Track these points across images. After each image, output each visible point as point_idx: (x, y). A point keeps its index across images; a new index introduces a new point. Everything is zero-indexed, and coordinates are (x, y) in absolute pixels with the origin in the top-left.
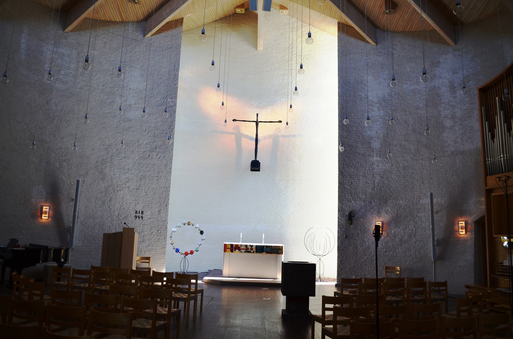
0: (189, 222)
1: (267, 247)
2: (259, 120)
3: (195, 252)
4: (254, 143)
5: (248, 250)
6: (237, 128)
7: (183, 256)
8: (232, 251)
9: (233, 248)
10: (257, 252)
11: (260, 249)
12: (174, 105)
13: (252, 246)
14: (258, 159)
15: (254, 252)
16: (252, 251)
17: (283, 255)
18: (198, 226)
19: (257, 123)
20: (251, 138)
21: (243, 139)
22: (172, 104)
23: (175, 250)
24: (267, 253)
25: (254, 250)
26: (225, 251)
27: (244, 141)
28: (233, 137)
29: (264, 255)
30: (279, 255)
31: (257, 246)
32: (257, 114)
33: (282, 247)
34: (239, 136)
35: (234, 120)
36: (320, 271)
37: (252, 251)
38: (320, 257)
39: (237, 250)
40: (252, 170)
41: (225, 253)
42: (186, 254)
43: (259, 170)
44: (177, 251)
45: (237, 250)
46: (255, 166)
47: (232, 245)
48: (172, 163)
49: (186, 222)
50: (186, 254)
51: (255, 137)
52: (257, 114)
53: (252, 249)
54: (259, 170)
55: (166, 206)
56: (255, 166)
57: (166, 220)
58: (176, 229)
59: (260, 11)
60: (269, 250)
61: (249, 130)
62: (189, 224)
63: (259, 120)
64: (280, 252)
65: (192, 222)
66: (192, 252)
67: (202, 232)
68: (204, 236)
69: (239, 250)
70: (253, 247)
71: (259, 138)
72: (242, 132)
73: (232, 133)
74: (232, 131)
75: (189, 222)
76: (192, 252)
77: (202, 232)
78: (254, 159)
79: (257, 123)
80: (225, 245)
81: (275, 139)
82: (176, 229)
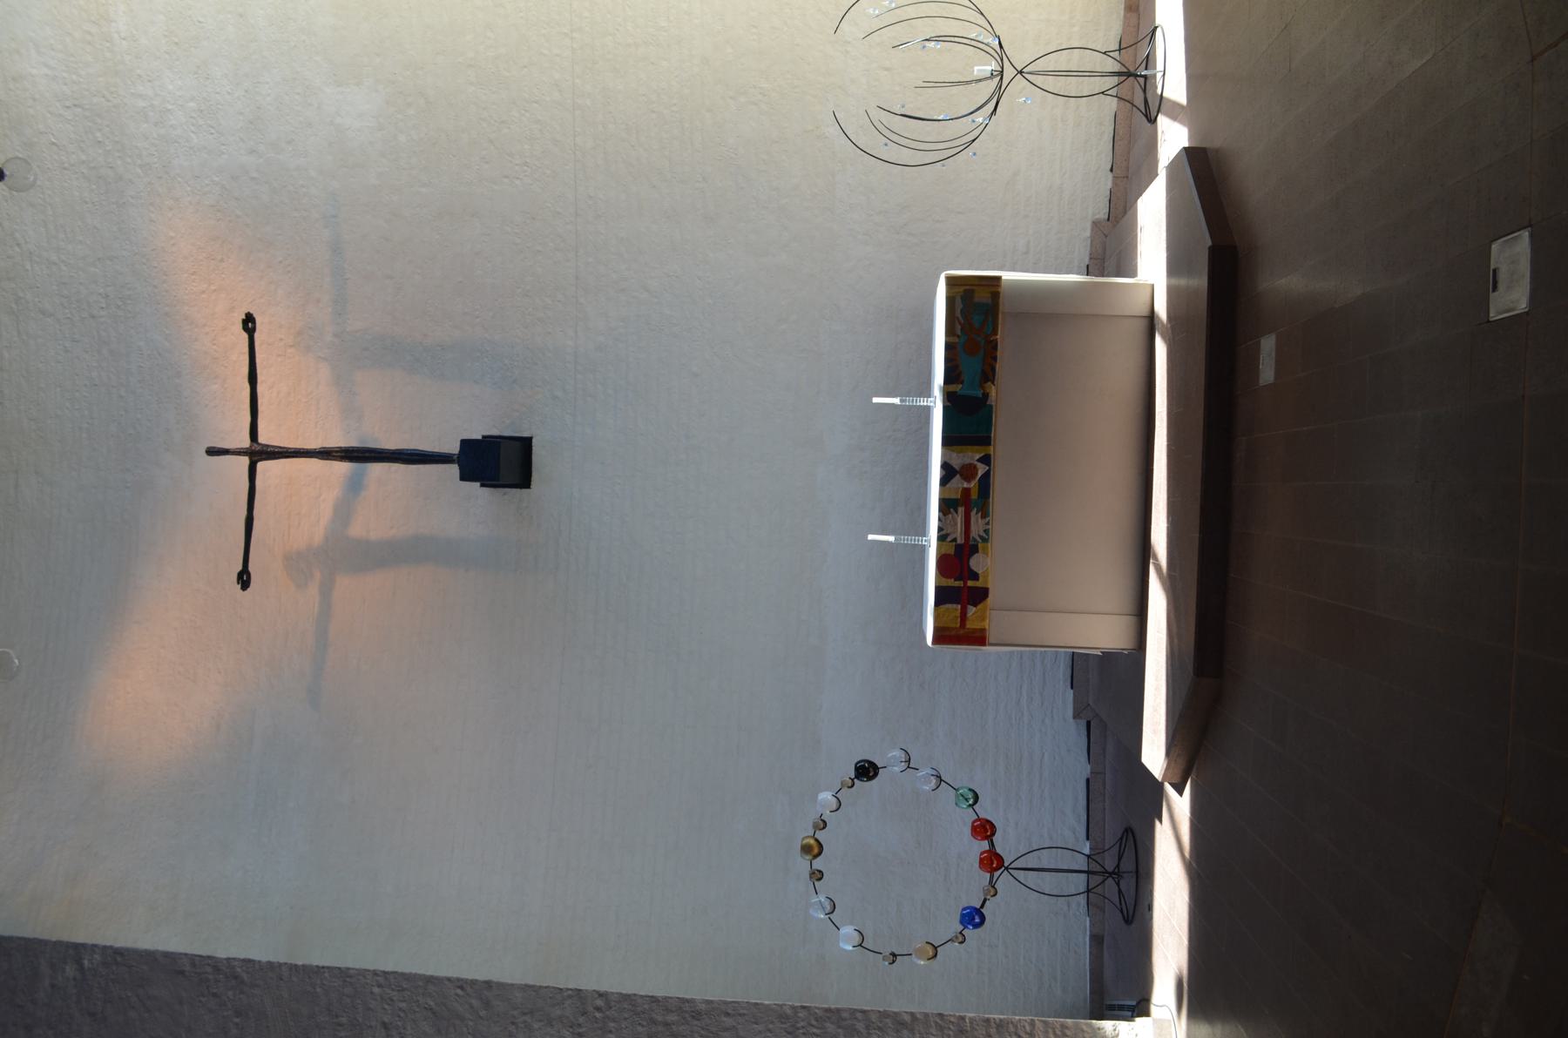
0: (806, 849)
1: (951, 375)
2: (246, 442)
3: (985, 810)
4: (376, 469)
5: (969, 496)
6: (298, 564)
7: (1004, 880)
8: (980, 595)
9: (962, 586)
10: (986, 441)
11: (969, 419)
12: (79, 962)
13: (948, 472)
14: (454, 448)
15: (986, 460)
16: (982, 469)
17: (1007, 276)
18: (826, 796)
19: (258, 453)
20: (355, 486)
21: (356, 530)
22: (70, 970)
23: (970, 932)
24: (988, 375)
25: (972, 455)
26: (979, 639)
27: (370, 524)
28: (344, 583)
29: (1004, 395)
30: (1004, 306)
31: (947, 442)
32: (212, 452)
33: (952, 282)
34: (345, 555)
35: (244, 579)
36: (1091, 74)
37: (982, 469)
38: (1009, 72)
39: (976, 563)
40: (524, 481)
41: (992, 636)
42: (992, 862)
43: (526, 444)
44: (973, 917)
45: (976, 563)
46: (498, 462)
47: (942, 596)
48: (430, 980)
49: (803, 865)
50: (992, 862)
51: (343, 468)
52: (212, 452)
53: (968, 472)
54: (526, 444)
55: (697, 1015)
56: (498, 462)
57: (783, 1017)
58: (848, 930)
59: (978, 584)
60: (971, 366)
61: (302, 498)
62: (813, 850)
63: (246, 442)
64: (982, 296)
65: (804, 832)
66: (984, 829)
67: (866, 771)
68: (888, 757)
69: (974, 549)
70: (956, 463)
71: (343, 443)
72: (318, 536)
73: (326, 592)
74: (313, 591)
75: (806, 849)
76: (984, 829)
77: (866, 771)
78: (454, 469)
79: (258, 453)
80: (941, 636)
81: (364, 353)
82: (848, 930)
